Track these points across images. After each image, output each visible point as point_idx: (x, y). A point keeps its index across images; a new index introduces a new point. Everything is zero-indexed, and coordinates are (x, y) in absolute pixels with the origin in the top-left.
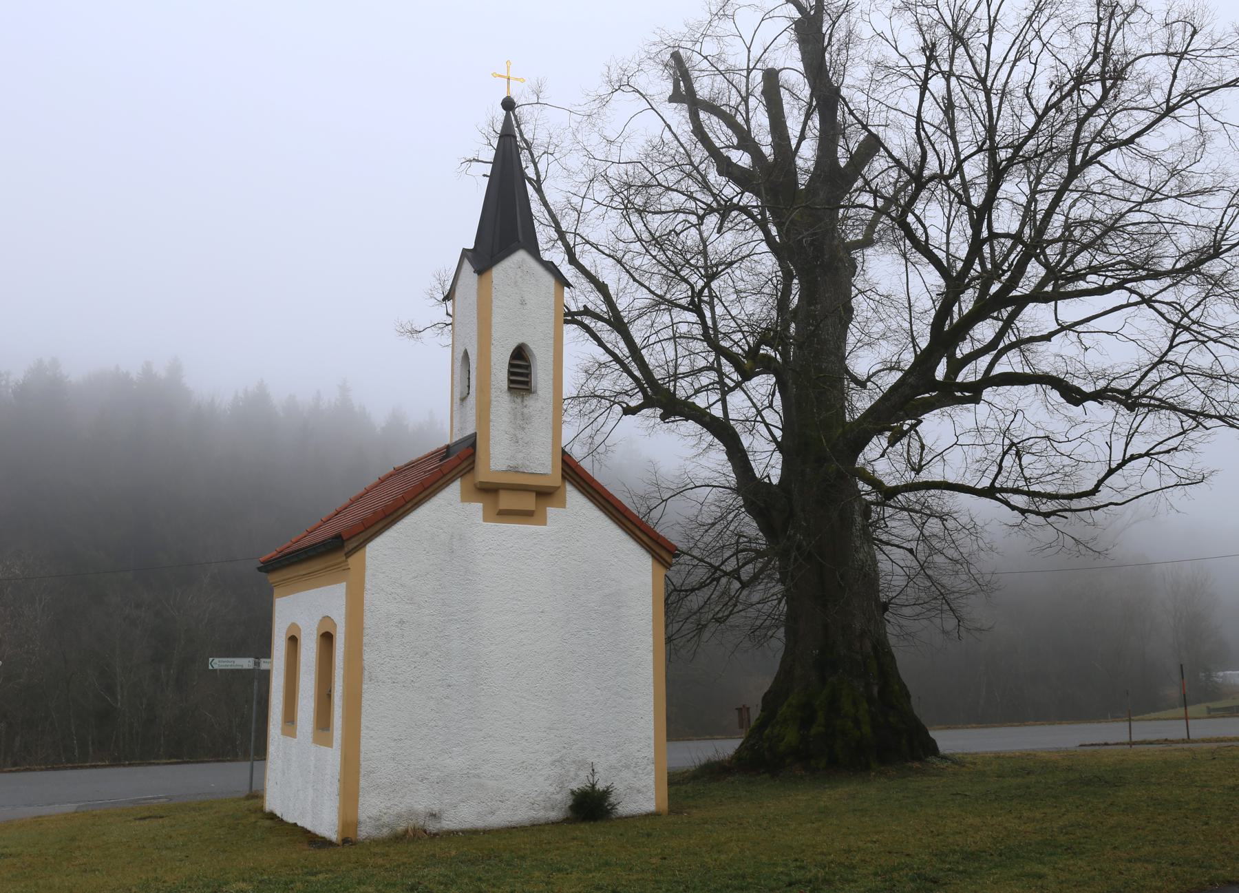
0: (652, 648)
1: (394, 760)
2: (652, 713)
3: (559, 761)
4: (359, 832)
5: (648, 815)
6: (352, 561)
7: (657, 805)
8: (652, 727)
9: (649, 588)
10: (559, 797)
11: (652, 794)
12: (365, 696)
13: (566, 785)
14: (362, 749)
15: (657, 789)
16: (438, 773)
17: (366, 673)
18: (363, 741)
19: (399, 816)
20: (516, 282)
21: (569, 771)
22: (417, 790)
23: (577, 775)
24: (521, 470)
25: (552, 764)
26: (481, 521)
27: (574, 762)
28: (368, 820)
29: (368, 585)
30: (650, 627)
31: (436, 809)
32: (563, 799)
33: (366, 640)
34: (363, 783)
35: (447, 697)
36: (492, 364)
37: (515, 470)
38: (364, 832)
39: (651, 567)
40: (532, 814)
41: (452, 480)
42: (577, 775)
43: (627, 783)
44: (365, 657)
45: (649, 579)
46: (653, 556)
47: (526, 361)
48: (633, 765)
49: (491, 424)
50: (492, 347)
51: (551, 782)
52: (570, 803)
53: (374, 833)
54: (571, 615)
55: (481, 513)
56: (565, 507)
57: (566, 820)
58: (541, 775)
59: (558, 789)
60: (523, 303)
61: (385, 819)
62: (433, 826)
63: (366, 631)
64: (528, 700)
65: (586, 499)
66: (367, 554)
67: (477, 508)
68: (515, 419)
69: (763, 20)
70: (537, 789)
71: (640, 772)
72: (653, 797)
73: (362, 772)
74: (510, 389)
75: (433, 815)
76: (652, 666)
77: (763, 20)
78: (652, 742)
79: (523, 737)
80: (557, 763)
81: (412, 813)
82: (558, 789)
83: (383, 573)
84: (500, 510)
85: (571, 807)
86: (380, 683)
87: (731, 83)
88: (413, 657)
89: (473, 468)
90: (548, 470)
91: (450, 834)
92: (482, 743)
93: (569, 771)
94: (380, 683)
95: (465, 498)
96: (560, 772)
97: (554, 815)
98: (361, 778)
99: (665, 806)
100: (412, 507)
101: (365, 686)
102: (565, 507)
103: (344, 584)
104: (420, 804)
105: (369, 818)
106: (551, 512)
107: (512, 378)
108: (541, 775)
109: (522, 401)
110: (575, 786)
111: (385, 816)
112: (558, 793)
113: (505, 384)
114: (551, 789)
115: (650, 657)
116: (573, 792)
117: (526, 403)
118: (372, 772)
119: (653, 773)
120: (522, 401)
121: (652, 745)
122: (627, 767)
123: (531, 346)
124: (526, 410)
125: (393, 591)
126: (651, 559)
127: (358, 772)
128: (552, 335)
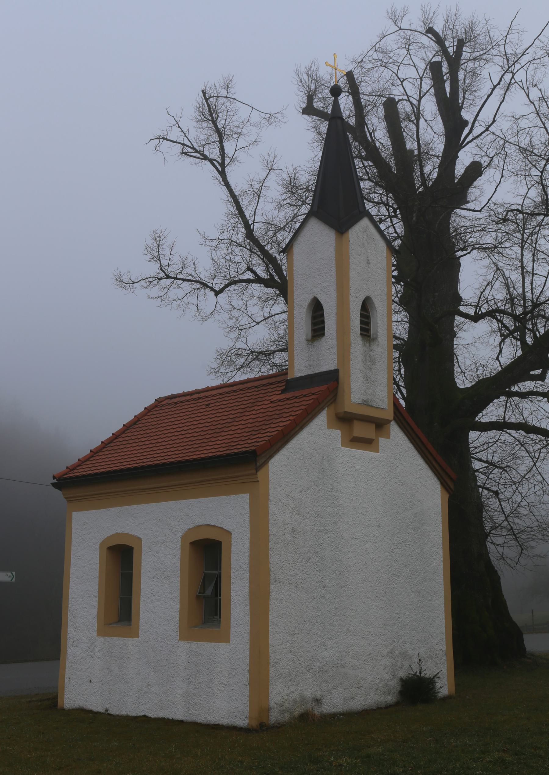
0: (442, 559)
4: (270, 717)
6: (260, 474)
10: (392, 683)
12: (272, 595)
13: (396, 673)
14: (271, 642)
16: (319, 664)
17: (272, 575)
18: (271, 635)
19: (295, 702)
20: (363, 244)
21: (398, 661)
22: (306, 678)
23: (402, 665)
27: (400, 653)
28: (275, 706)
29: (271, 497)
30: (441, 542)
31: (318, 694)
32: (395, 685)
33: (271, 545)
34: (272, 673)
35: (323, 597)
36: (351, 311)
37: (366, 404)
38: (274, 717)
39: (440, 492)
40: (377, 698)
41: (323, 409)
42: (402, 665)
44: (271, 560)
46: (442, 484)
48: (434, 656)
49: (351, 362)
50: (350, 297)
52: (399, 689)
54: (395, 530)
56: (389, 438)
57: (397, 704)
59: (392, 677)
60: (368, 262)
62: (318, 711)
66: (270, 469)
67: (337, 433)
68: (365, 360)
69: (235, 151)
70: (378, 677)
71: (438, 662)
73: (272, 663)
74: (361, 334)
75: (317, 701)
77: (235, 151)
79: (370, 632)
82: (392, 677)
84: (354, 437)
85: (400, 692)
86: (281, 584)
87: (428, 125)
89: (335, 400)
91: (333, 717)
93: (398, 661)
94: (281, 584)
95: (330, 426)
96: (392, 662)
97: (390, 699)
98: (271, 669)
99: (453, 691)
101: (272, 587)
102: (389, 438)
103: (247, 496)
104: (308, 691)
105: (276, 704)
106: (382, 441)
109: (370, 346)
110: (402, 674)
111: (287, 702)
112: (392, 680)
113: (359, 332)
114: (388, 677)
116: (401, 679)
117: (372, 347)
120: (370, 346)
123: (374, 300)
127: (268, 663)
128: (385, 292)
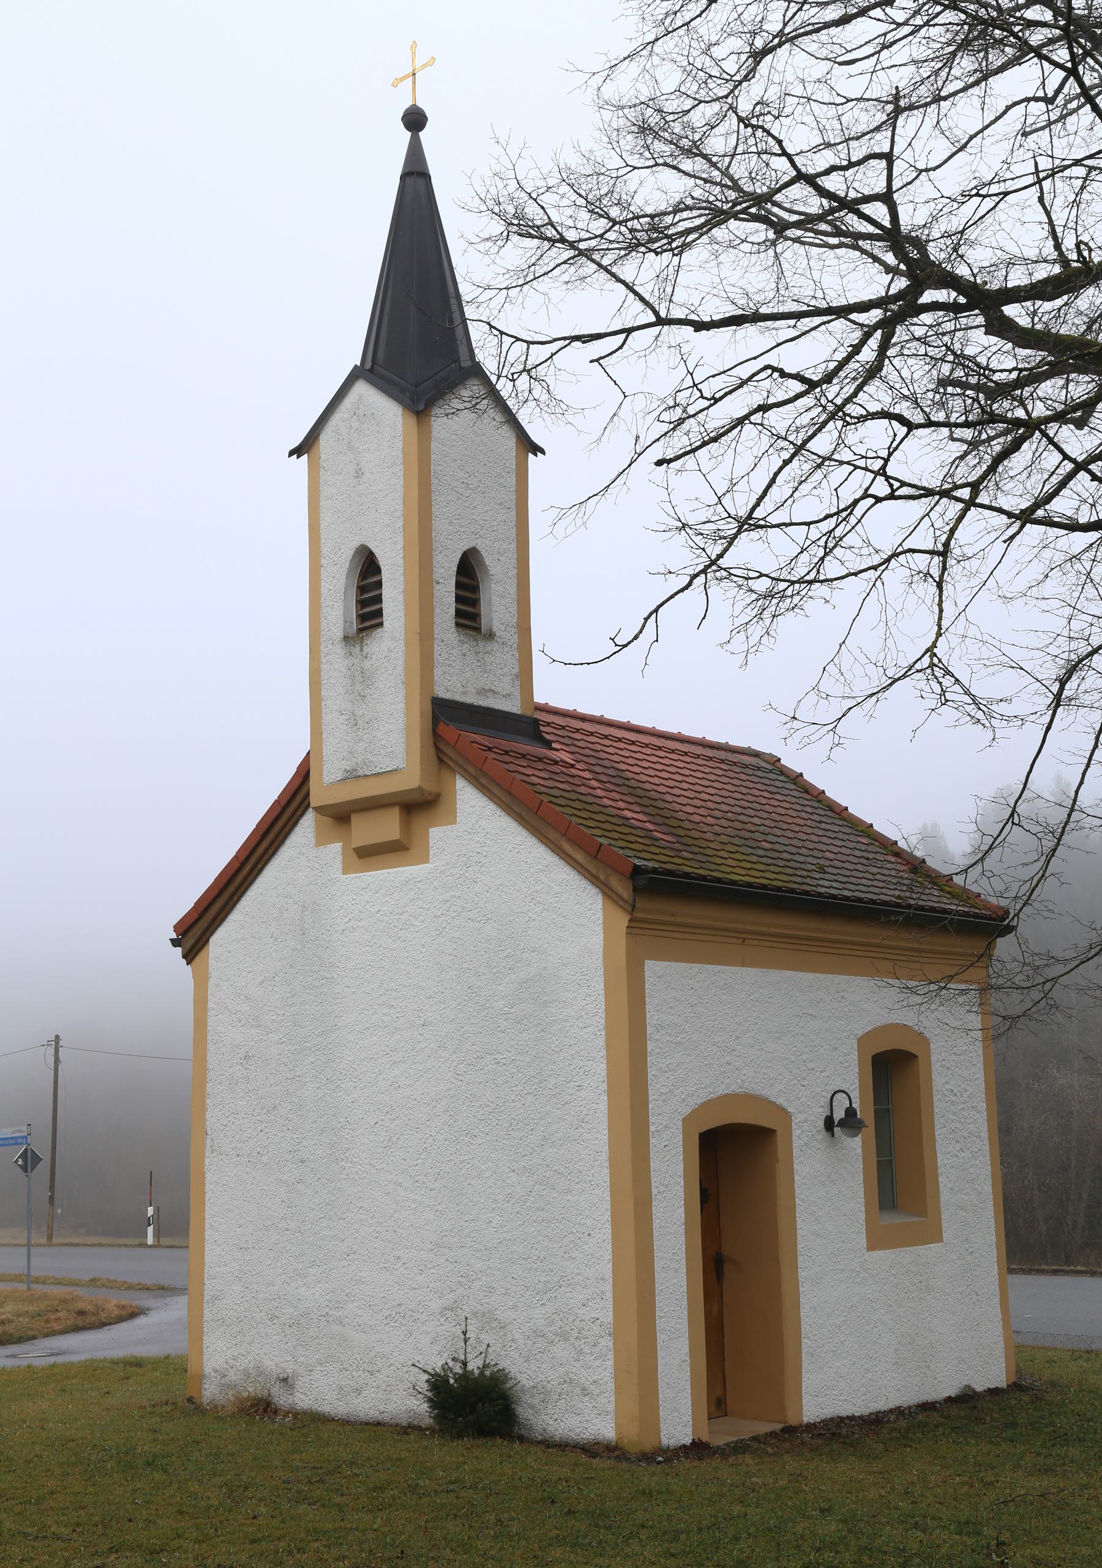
1: (240, 1281)
2: (608, 1226)
3: (451, 1310)
5: (592, 1449)
7: (618, 1427)
8: (608, 1256)
9: (598, 960)
11: (608, 1400)
15: (619, 1391)
24: (361, 773)
25: (441, 1314)
26: (339, 875)
28: (213, 1374)
30: (601, 1042)
39: (600, 915)
43: (562, 1370)
45: (595, 939)
46: (605, 894)
47: (473, 580)
48: (574, 1334)
51: (439, 1348)
53: (221, 1399)
55: (339, 859)
58: (427, 1333)
61: (232, 1376)
63: (211, 1075)
64: (406, 1189)
65: (485, 799)
68: (353, 684)
71: (586, 1349)
72: (611, 1407)
73: (206, 1298)
76: (605, 1125)
78: (608, 1287)
80: (449, 1313)
81: (260, 1371)
83: (227, 980)
88: (259, 1114)
90: (398, 761)
92: (344, 1263)
100: (591, 874)
101: (207, 1161)
105: (215, 1371)
106: (437, 835)
107: (461, 621)
108: (427, 1333)
115: (603, 1105)
117: (366, 649)
118: (217, 1298)
119: (611, 1356)
120: (362, 650)
121: (609, 1295)
122: (564, 1336)
124: (367, 664)
125: (238, 1008)
126: (600, 896)
